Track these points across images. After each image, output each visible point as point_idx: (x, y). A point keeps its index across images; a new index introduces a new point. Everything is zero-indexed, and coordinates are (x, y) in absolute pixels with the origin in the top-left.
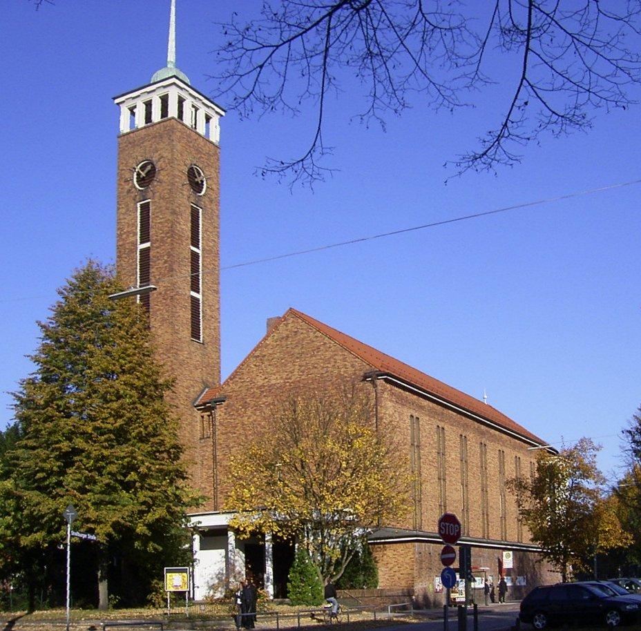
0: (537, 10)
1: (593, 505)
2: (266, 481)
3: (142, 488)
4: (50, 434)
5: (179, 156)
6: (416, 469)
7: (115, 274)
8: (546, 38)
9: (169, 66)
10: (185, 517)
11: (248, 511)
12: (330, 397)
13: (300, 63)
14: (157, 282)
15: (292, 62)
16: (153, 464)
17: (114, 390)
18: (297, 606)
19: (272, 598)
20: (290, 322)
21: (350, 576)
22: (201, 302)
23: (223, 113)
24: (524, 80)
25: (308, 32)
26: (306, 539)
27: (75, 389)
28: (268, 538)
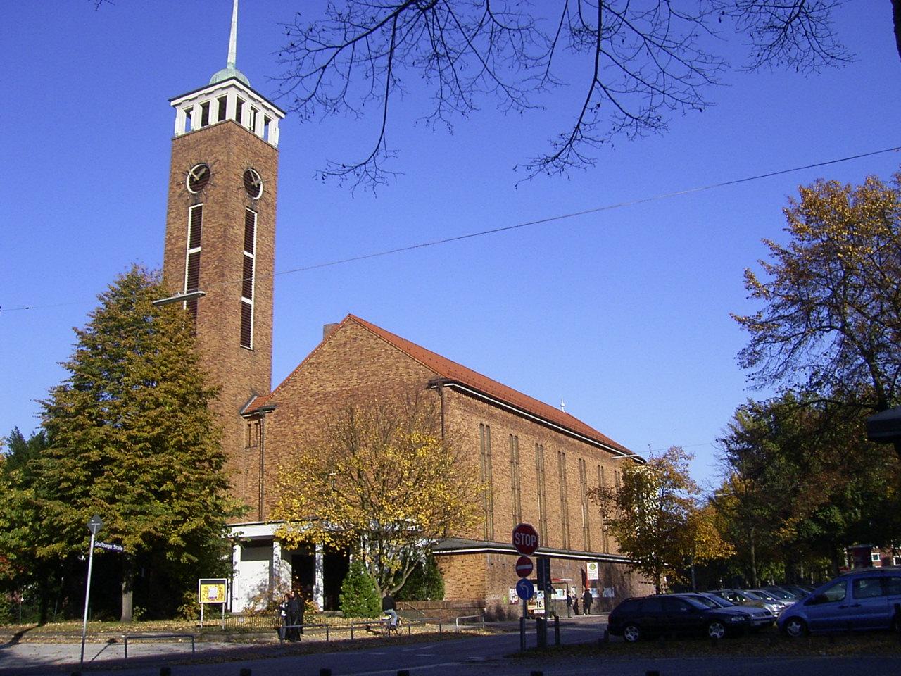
0: (607, 10)
1: (687, 515)
2: (318, 490)
3: (178, 498)
4: (79, 442)
5: (236, 158)
6: (487, 478)
7: (161, 279)
8: (617, 39)
9: (228, 67)
10: (225, 528)
11: (297, 521)
12: (390, 405)
13: (364, 64)
14: (206, 288)
15: (356, 63)
16: (192, 473)
17: (153, 398)
18: (351, 619)
19: (321, 610)
20: (348, 328)
21: (412, 588)
22: (252, 308)
23: (283, 116)
24: (596, 82)
25: (373, 33)
26: (362, 549)
27: (110, 396)
28: (319, 548)
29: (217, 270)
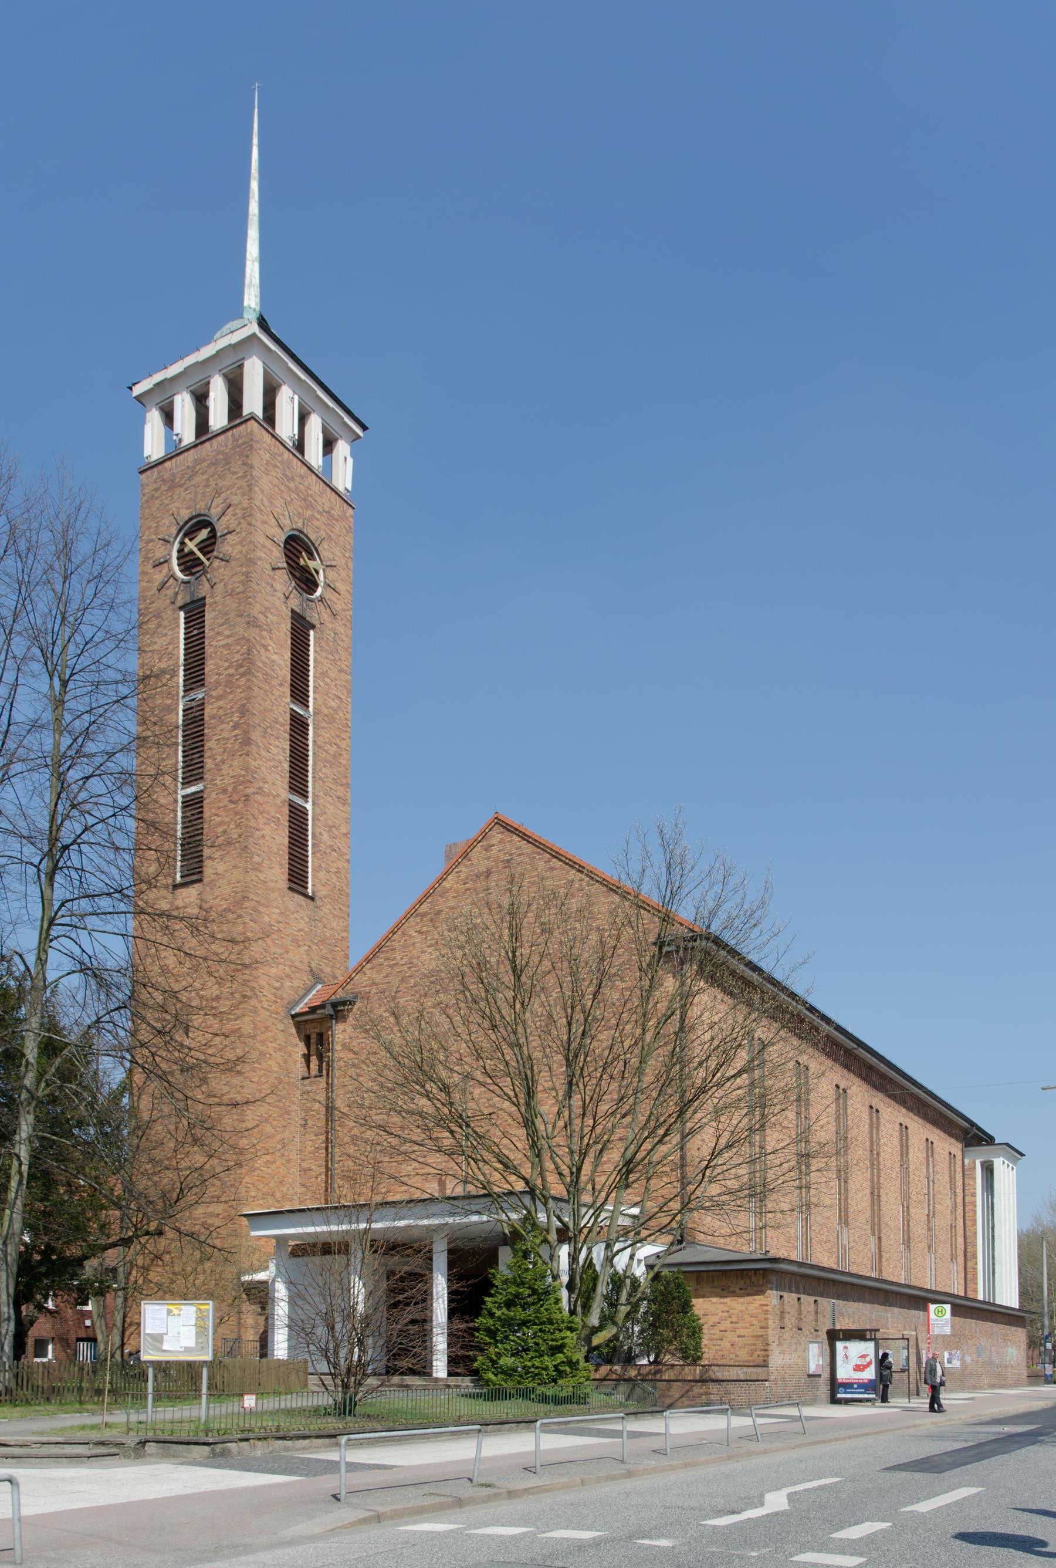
5: (266, 503)
9: (245, 315)
20: (495, 841)
29: (237, 732)
